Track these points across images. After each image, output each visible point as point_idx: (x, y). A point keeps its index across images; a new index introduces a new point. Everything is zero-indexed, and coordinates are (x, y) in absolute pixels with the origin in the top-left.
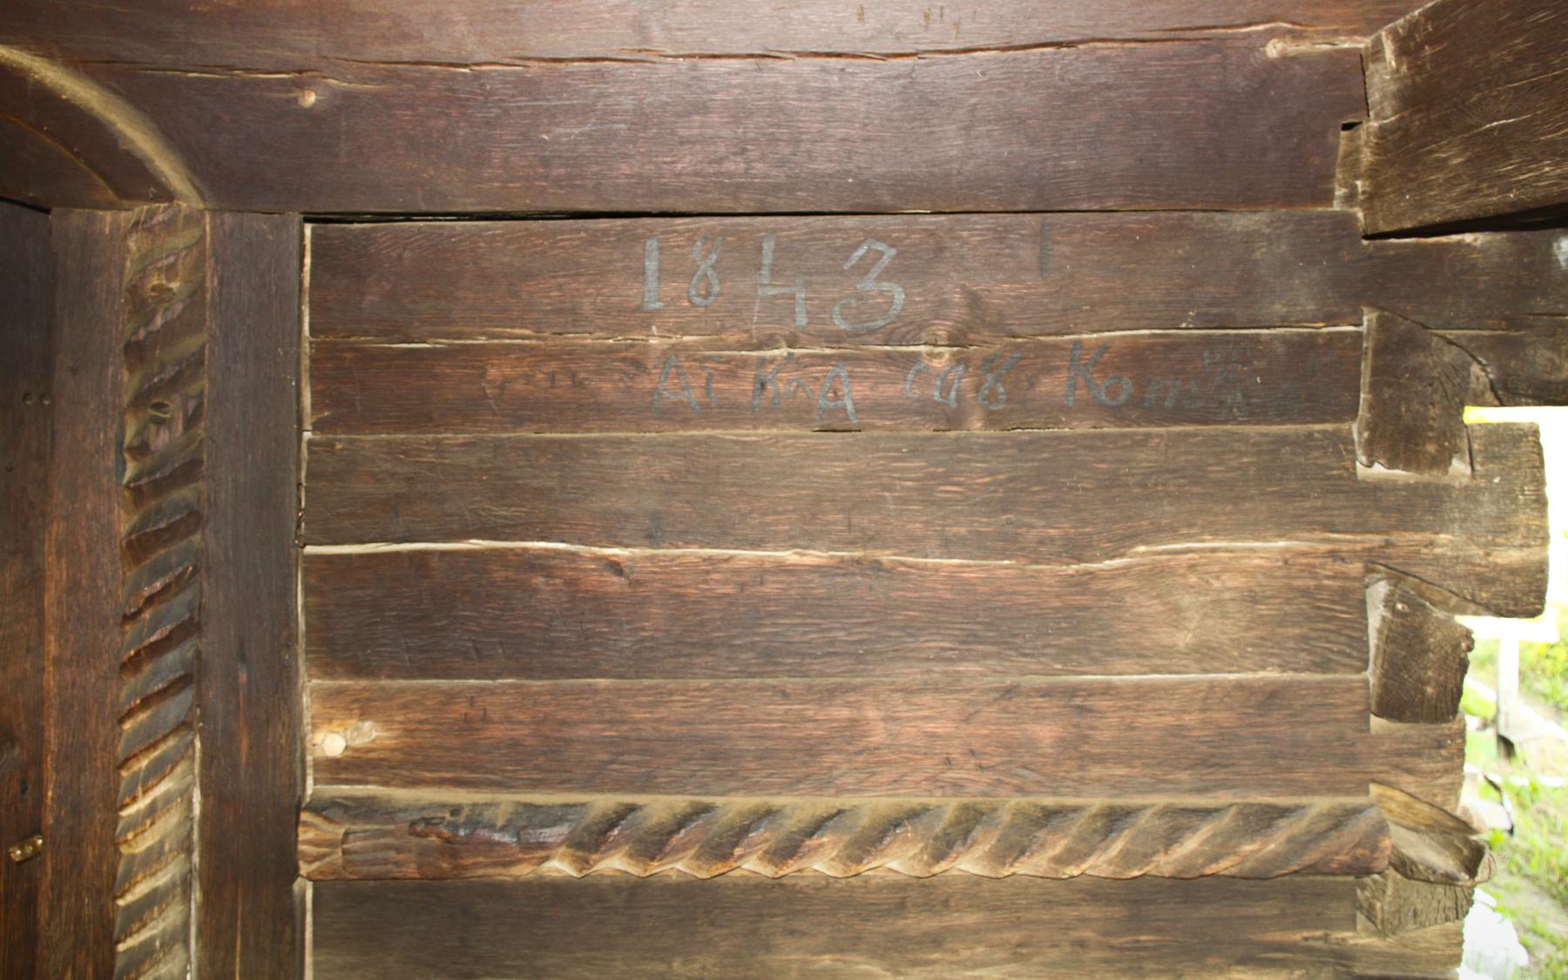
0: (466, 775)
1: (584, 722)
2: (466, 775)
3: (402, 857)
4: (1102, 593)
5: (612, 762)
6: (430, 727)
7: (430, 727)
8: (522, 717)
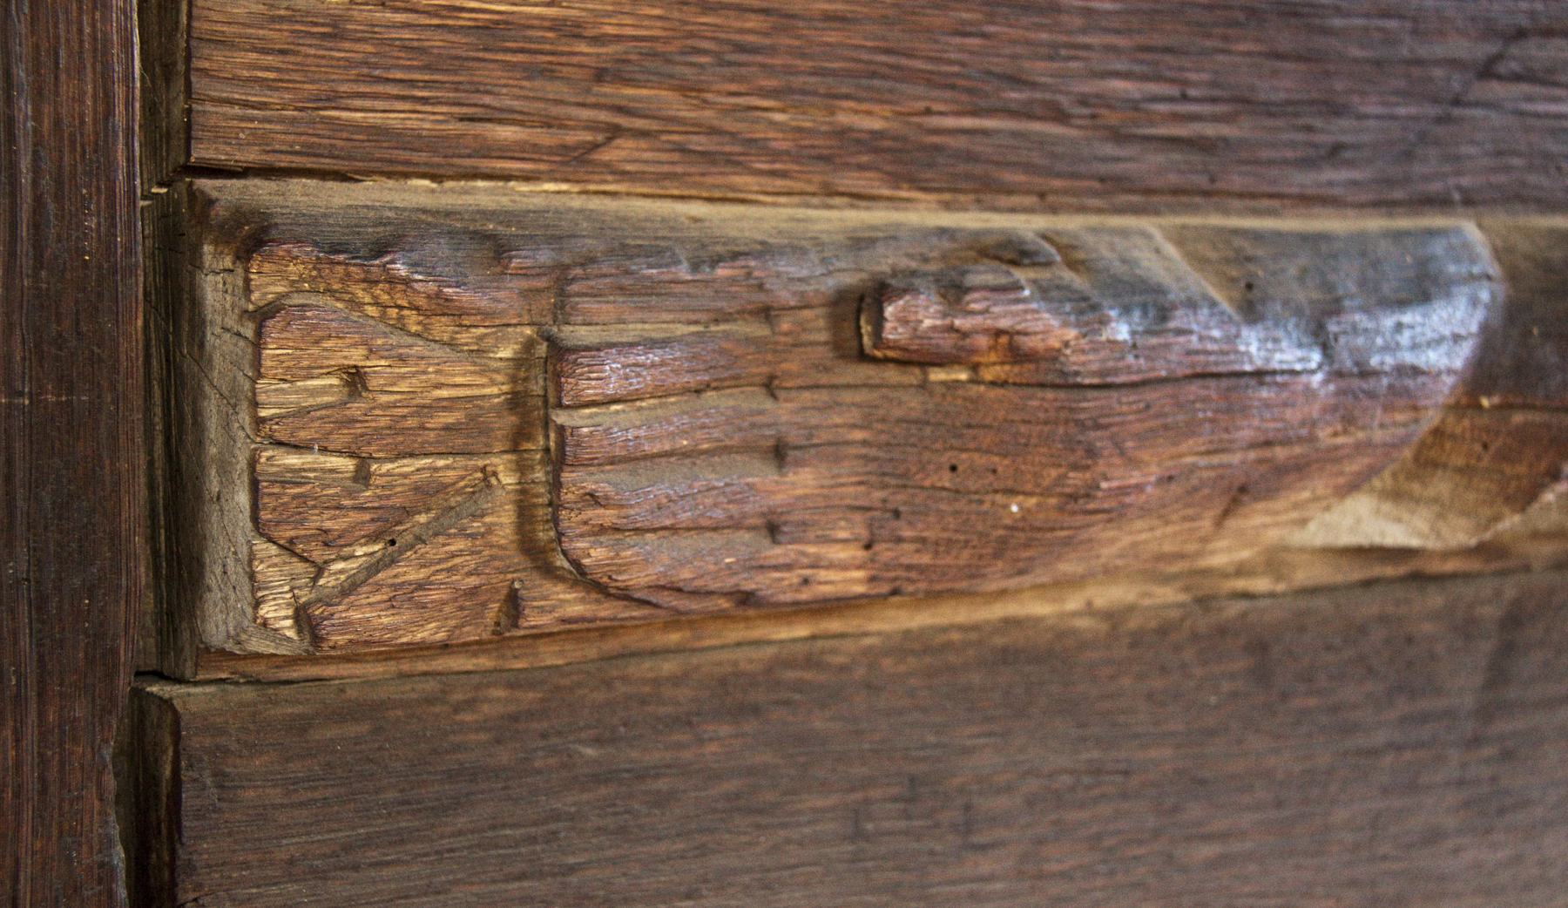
3: (803, 481)
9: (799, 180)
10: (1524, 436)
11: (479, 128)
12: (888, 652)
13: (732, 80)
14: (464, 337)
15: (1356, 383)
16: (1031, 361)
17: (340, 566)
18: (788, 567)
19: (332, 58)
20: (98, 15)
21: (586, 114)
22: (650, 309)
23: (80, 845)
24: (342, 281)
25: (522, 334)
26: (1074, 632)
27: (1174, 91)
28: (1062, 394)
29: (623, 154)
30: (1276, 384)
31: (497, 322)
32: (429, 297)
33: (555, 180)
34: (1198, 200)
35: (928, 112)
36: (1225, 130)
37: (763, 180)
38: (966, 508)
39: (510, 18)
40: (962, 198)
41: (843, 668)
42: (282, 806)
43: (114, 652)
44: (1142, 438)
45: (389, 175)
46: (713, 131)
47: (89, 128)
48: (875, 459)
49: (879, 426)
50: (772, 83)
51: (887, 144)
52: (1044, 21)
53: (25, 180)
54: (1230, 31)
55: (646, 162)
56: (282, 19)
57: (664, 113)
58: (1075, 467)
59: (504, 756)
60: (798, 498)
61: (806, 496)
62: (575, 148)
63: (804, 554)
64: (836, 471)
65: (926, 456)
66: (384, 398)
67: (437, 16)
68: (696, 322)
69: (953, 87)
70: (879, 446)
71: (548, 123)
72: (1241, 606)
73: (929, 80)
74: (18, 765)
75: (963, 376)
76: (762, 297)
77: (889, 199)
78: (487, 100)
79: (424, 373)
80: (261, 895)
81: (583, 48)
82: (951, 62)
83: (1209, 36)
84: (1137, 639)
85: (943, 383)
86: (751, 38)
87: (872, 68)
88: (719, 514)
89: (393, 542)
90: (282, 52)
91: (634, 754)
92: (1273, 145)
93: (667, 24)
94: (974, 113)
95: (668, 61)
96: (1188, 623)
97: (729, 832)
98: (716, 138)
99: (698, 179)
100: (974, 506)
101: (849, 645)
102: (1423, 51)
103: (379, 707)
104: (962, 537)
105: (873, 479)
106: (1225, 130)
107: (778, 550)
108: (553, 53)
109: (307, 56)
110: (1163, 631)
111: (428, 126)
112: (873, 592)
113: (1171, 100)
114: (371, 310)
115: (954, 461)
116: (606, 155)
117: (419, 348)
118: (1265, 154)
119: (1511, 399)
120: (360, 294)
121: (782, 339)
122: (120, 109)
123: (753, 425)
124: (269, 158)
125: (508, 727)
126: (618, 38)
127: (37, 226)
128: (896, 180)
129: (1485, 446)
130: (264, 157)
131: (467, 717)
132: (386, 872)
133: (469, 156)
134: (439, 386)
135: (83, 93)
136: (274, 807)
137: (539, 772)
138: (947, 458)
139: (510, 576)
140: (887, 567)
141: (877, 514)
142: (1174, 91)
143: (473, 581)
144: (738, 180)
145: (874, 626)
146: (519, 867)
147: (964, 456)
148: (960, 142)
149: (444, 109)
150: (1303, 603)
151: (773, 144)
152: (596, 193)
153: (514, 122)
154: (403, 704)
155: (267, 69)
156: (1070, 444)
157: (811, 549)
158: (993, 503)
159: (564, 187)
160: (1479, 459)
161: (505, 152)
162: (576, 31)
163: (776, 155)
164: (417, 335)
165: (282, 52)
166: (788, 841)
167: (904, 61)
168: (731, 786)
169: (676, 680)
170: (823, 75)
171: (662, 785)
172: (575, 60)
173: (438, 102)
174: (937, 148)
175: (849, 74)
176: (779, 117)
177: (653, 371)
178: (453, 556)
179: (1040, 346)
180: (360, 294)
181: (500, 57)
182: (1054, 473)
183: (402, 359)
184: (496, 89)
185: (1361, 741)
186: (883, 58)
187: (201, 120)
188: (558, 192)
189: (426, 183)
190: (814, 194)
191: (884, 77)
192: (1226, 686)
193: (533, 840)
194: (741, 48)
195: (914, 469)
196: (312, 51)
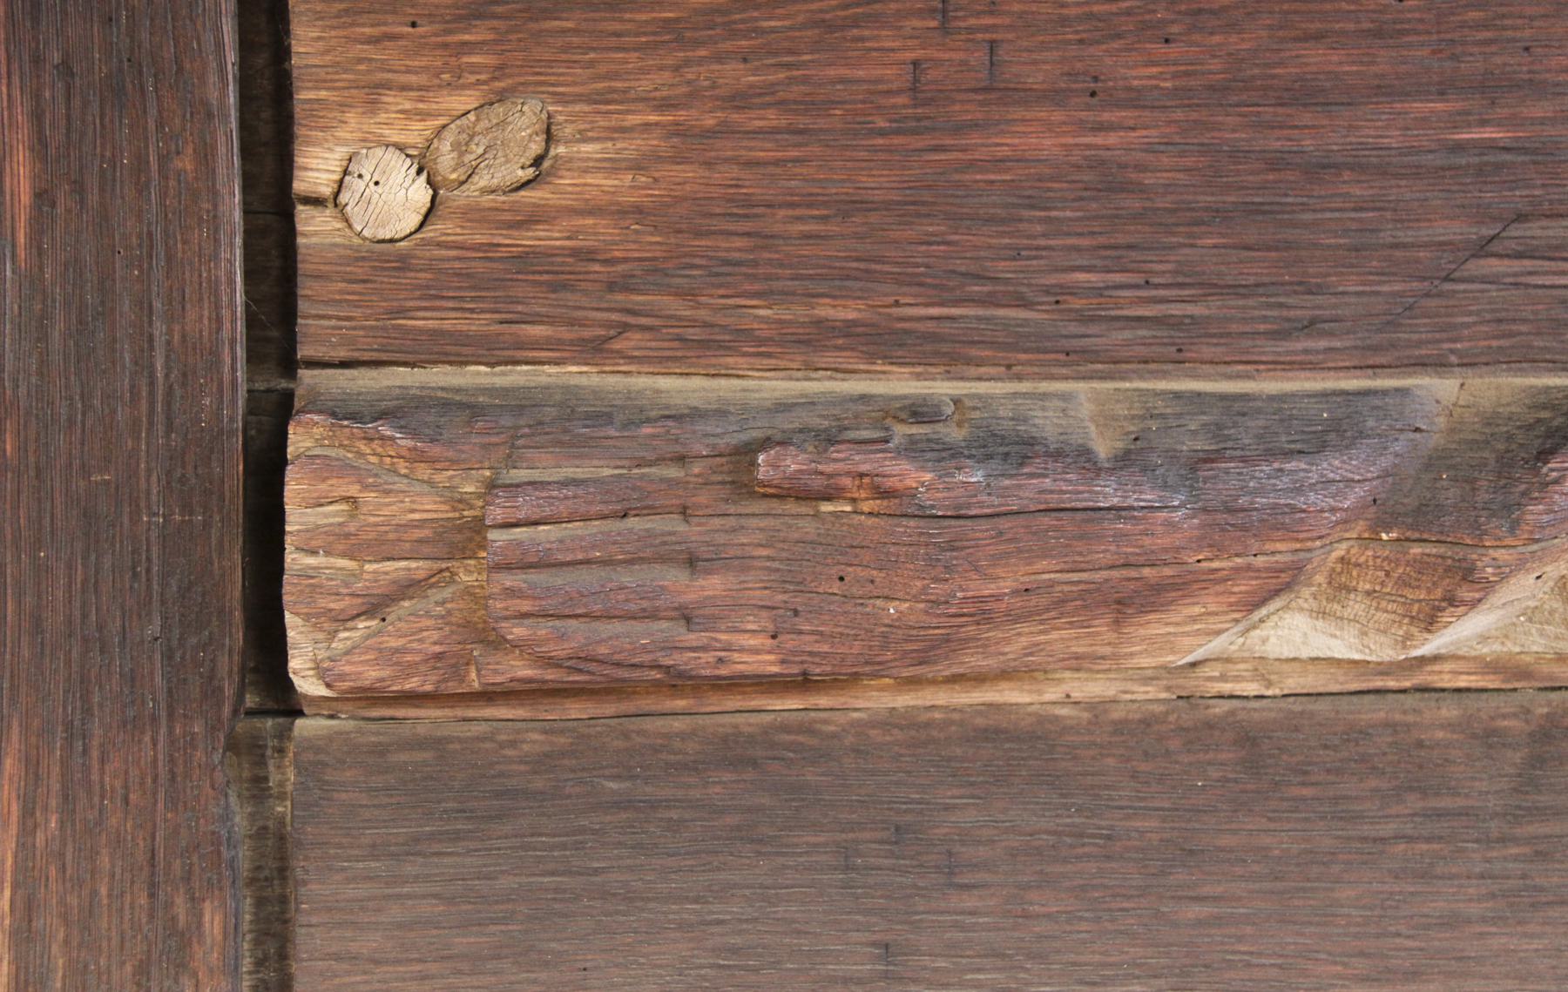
0: (917, 311)
1: (1383, 90)
2: (917, 311)
3: (713, 585)
4: (442, 496)
5: (1482, 249)
6: (772, 118)
7: (772, 118)
8: (1139, 75)
9: (782, 359)
10: (1421, 565)
11: (514, 327)
12: (872, 724)
13: (720, 286)
14: (438, 477)
15: (1221, 518)
16: (896, 497)
17: (346, 634)
18: (704, 649)
19: (401, 284)
20: (212, 265)
21: (599, 315)
22: (580, 456)
23: (198, 818)
24: (349, 438)
25: (483, 476)
26: (1057, 718)
27: (1138, 279)
28: (922, 523)
29: (632, 344)
30: (1134, 518)
31: (463, 466)
32: (409, 449)
33: (578, 364)
34: (1170, 367)
35: (897, 304)
36: (1191, 309)
37: (752, 360)
38: (853, 610)
39: (538, 250)
40: (932, 369)
41: (834, 736)
42: (366, 806)
43: (221, 689)
44: (996, 559)
45: (451, 363)
46: (706, 325)
47: (205, 340)
48: (778, 570)
49: (781, 545)
50: (757, 287)
51: (860, 330)
52: (1007, 229)
53: (160, 375)
54: (1195, 229)
55: (650, 349)
56: (364, 258)
57: (663, 313)
58: (936, 580)
59: (539, 783)
60: (706, 598)
61: (714, 597)
62: (592, 341)
63: (716, 640)
64: (742, 579)
65: (819, 568)
66: (372, 519)
67: (479, 250)
68: (623, 467)
69: (921, 284)
70: (781, 560)
71: (572, 323)
72: (1227, 705)
73: (899, 280)
74: (155, 760)
75: (848, 508)
76: (678, 448)
77: (868, 372)
78: (520, 308)
79: (402, 502)
80: (350, 868)
81: (597, 267)
82: (918, 265)
83: (1174, 234)
84: (1120, 727)
85: (831, 513)
86: (737, 255)
87: (845, 272)
88: (633, 607)
89: (384, 620)
90: (364, 281)
91: (649, 789)
92: (1244, 320)
93: (664, 248)
94: (942, 304)
95: (667, 275)
96: (1172, 718)
97: (731, 854)
98: (708, 330)
99: (694, 360)
100: (860, 608)
101: (840, 718)
102: (1406, 236)
103: (440, 741)
104: (853, 632)
105: (774, 585)
106: (1191, 309)
107: (692, 636)
108: (571, 273)
109: (382, 283)
110: (1147, 722)
111: (474, 328)
112: (786, 672)
113: (1136, 287)
114: (373, 459)
115: (841, 574)
116: (616, 345)
117: (402, 484)
118: (1234, 328)
119: (1409, 534)
120: (363, 447)
121: (692, 479)
122: (227, 325)
123: (665, 543)
124: (356, 355)
125: (543, 762)
126: (625, 260)
127: (168, 404)
128: (871, 357)
129: (1388, 574)
130: (350, 353)
131: (509, 752)
132: (446, 860)
133: (508, 349)
134: (413, 511)
135: (201, 317)
136: (361, 806)
137: (569, 796)
138: (835, 571)
139: (469, 646)
140: (794, 653)
141: (781, 612)
142: (1138, 279)
143: (438, 649)
144: (730, 360)
145: (860, 704)
146: (551, 866)
147: (850, 569)
148: (930, 326)
149: (488, 316)
150: (1296, 706)
151: (757, 333)
152: (613, 372)
153: (541, 323)
154: (459, 740)
155: (353, 293)
156: (931, 562)
157: (723, 637)
158: (874, 606)
159: (585, 369)
160: (1382, 584)
161: (536, 345)
162: (590, 256)
163: (761, 342)
164: (405, 476)
165: (364, 281)
166: (785, 867)
167: (874, 267)
168: (732, 820)
169: (683, 736)
170: (802, 280)
171: (674, 815)
172: (592, 277)
173: (483, 311)
174: (906, 332)
175: (823, 277)
176: (762, 312)
177: (566, 502)
178: (422, 630)
179: (899, 485)
180: (363, 447)
181: (531, 277)
182: (919, 584)
183: (387, 492)
184: (528, 300)
185: (1367, 830)
186: (855, 265)
187: (304, 330)
188: (581, 373)
189: (482, 368)
190: (799, 370)
191: (856, 279)
192: (1214, 773)
193: (564, 846)
194: (727, 262)
195: (809, 579)
196: (386, 280)
